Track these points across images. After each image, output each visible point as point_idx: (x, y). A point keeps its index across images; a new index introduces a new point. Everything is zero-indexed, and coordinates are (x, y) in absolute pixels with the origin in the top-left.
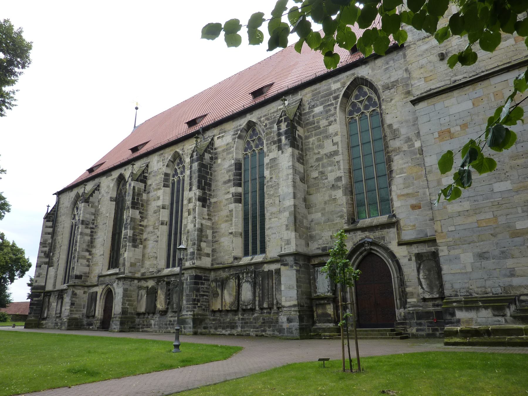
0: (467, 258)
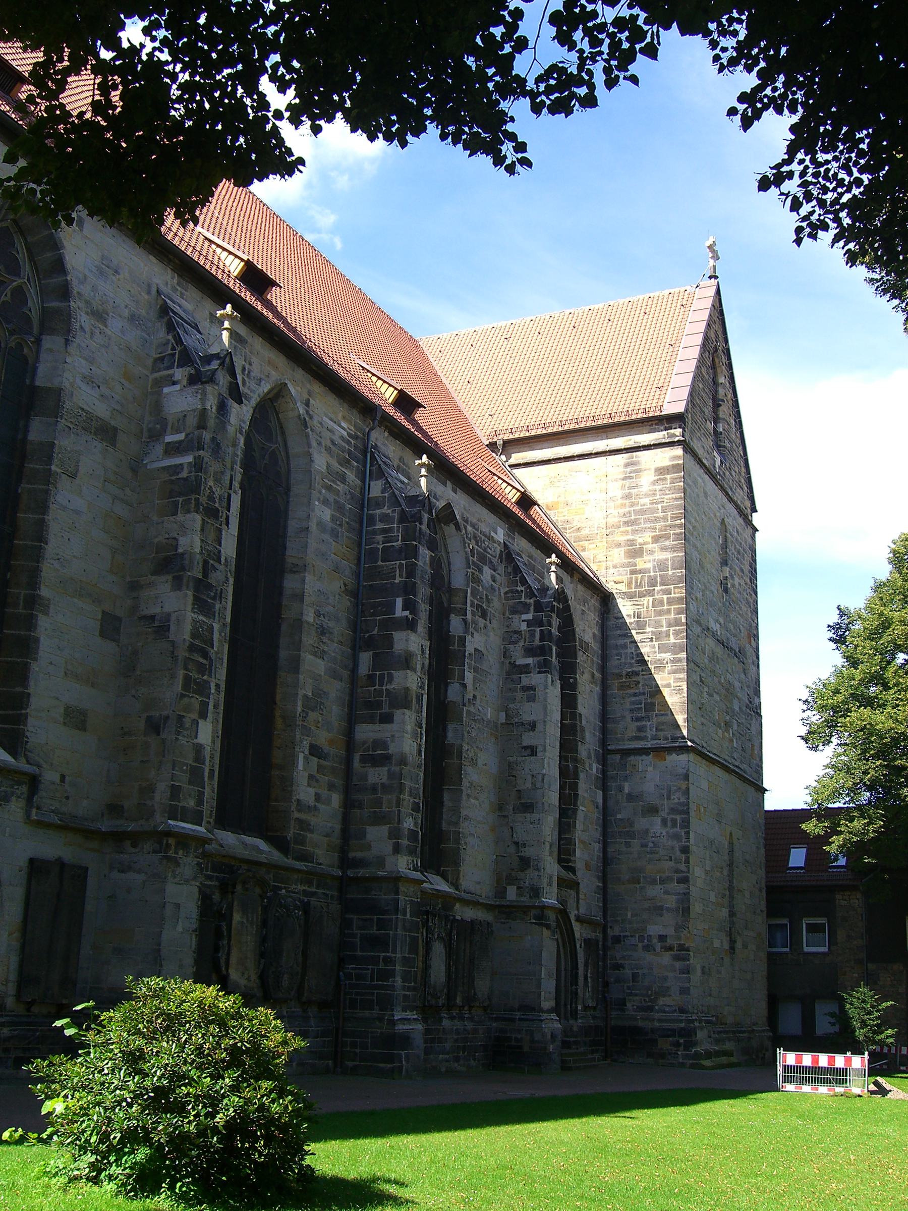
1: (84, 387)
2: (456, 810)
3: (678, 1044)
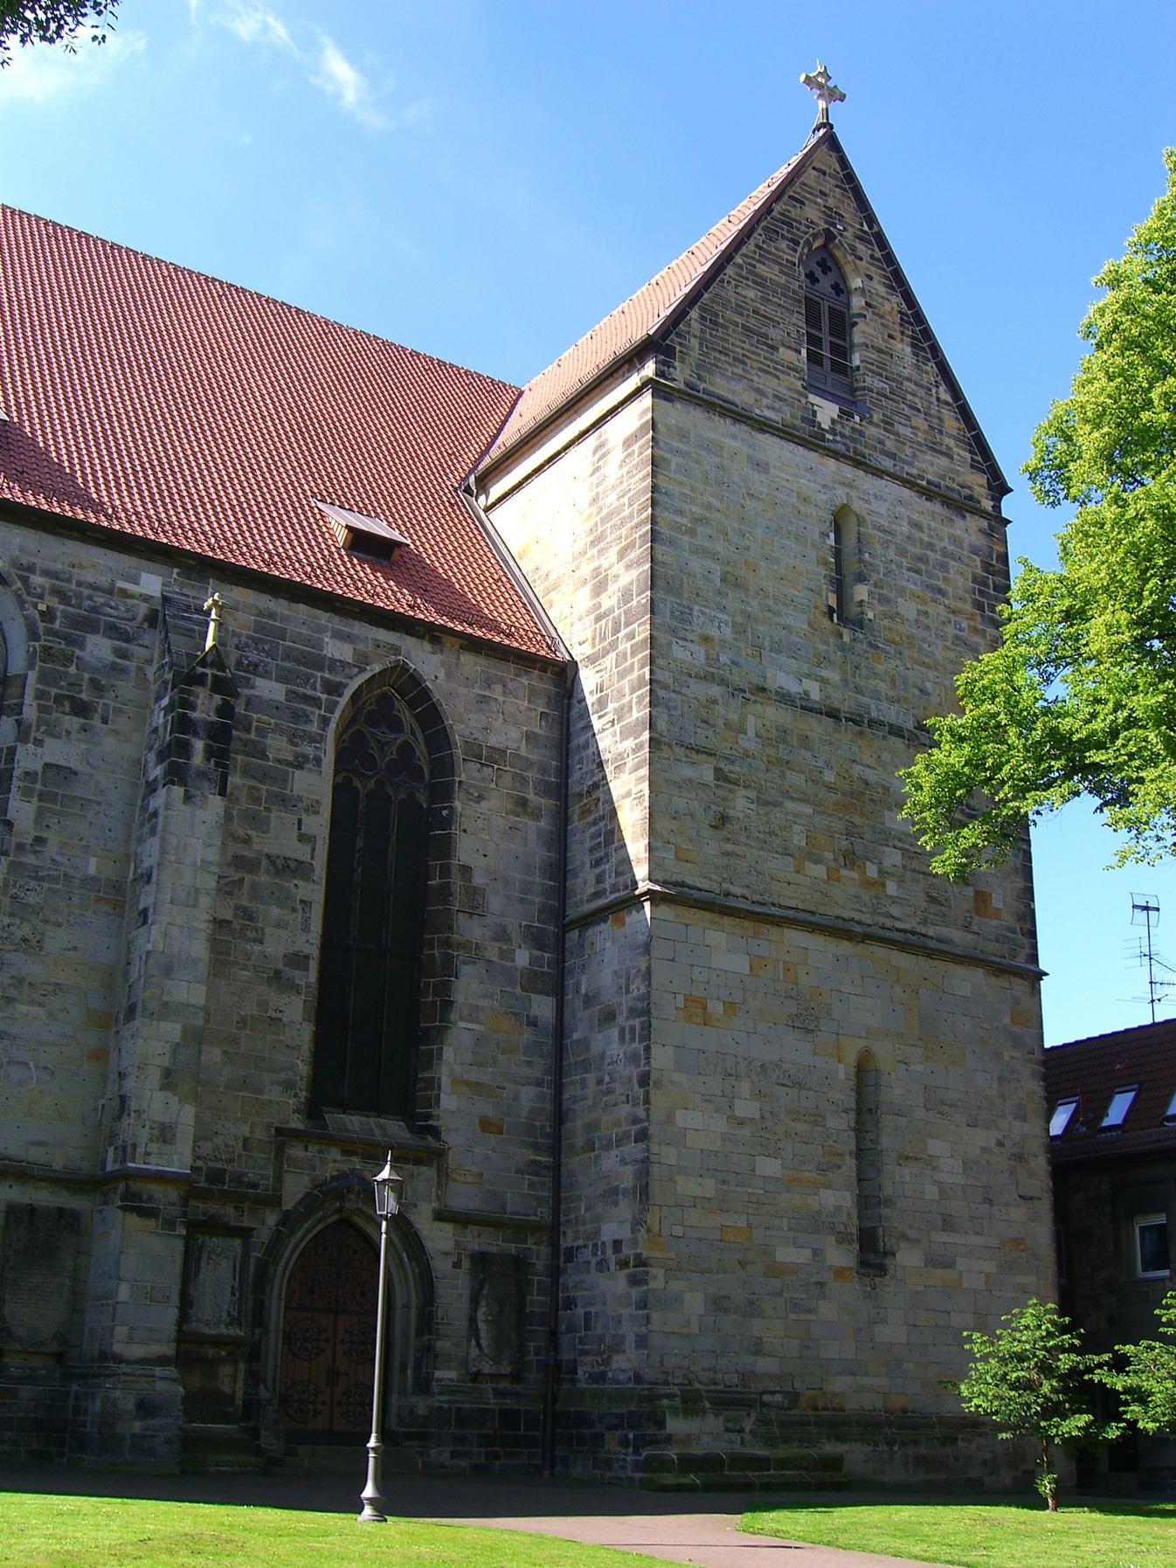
0: (695, 1303)
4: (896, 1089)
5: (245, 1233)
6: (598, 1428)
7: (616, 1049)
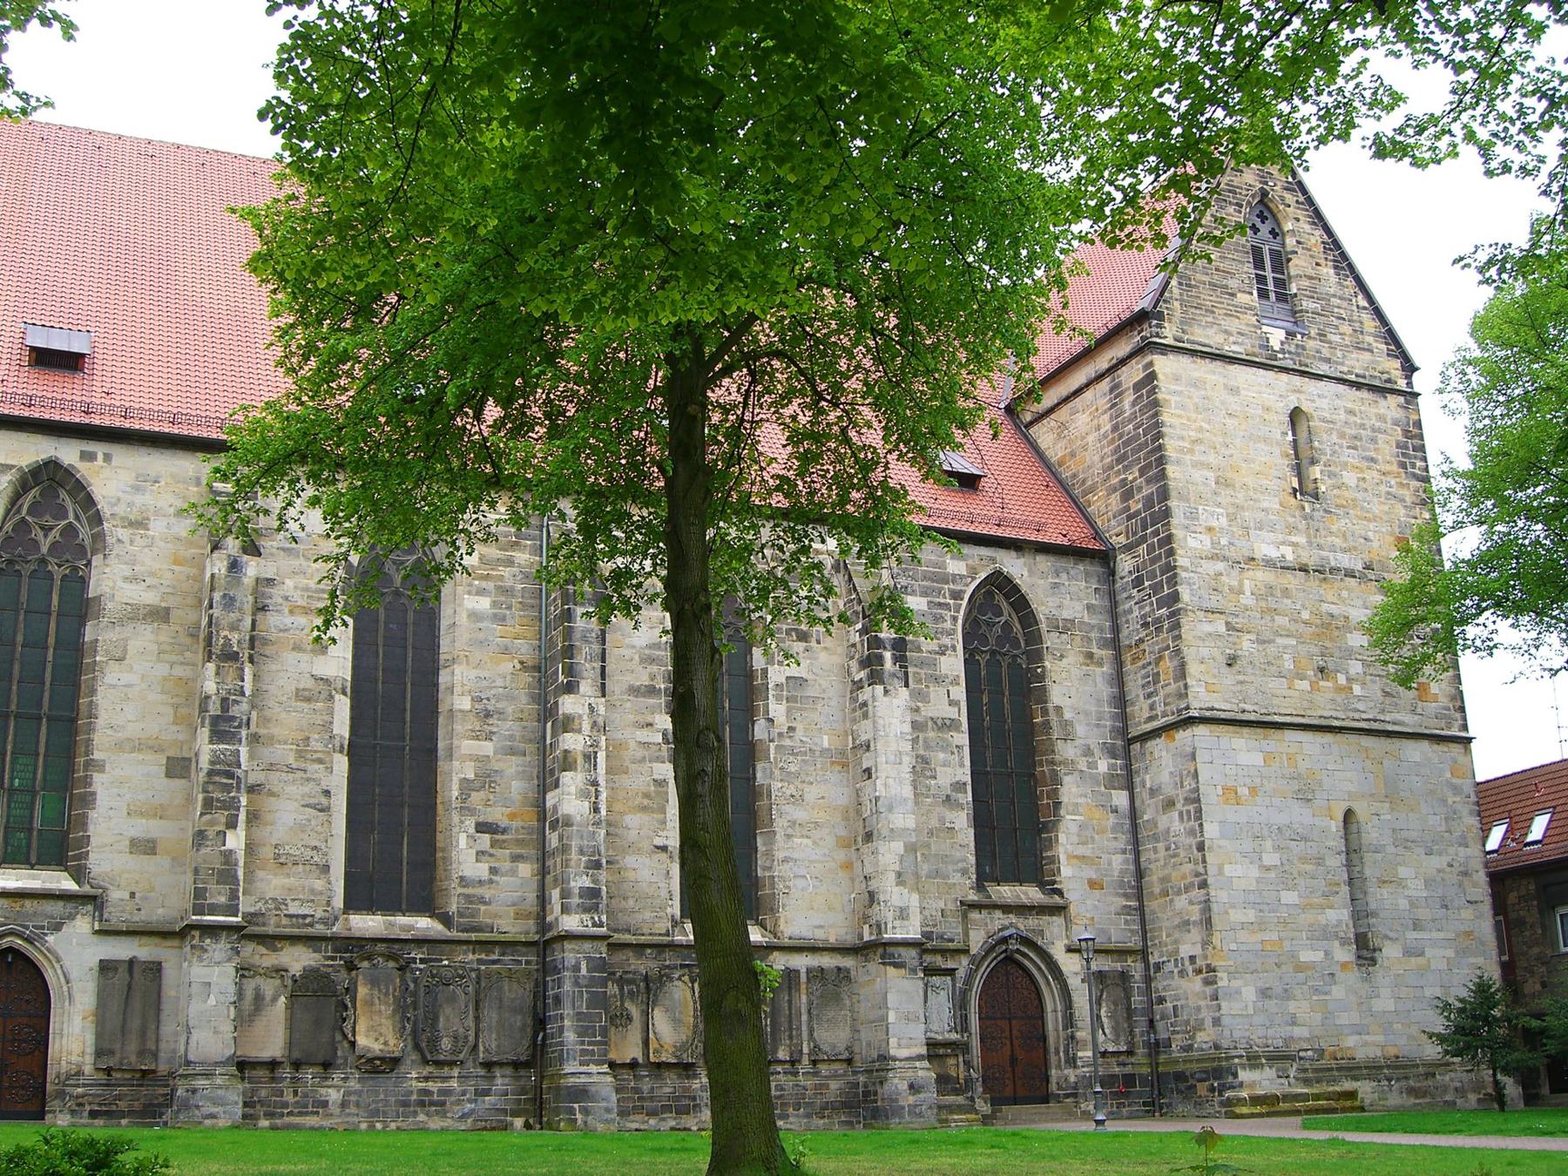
0: (1249, 994)
1: (126, 586)
2: (769, 854)
3: (1212, 1089)
4: (1372, 832)
5: (951, 972)
6: (1191, 1082)
7: (1177, 826)
